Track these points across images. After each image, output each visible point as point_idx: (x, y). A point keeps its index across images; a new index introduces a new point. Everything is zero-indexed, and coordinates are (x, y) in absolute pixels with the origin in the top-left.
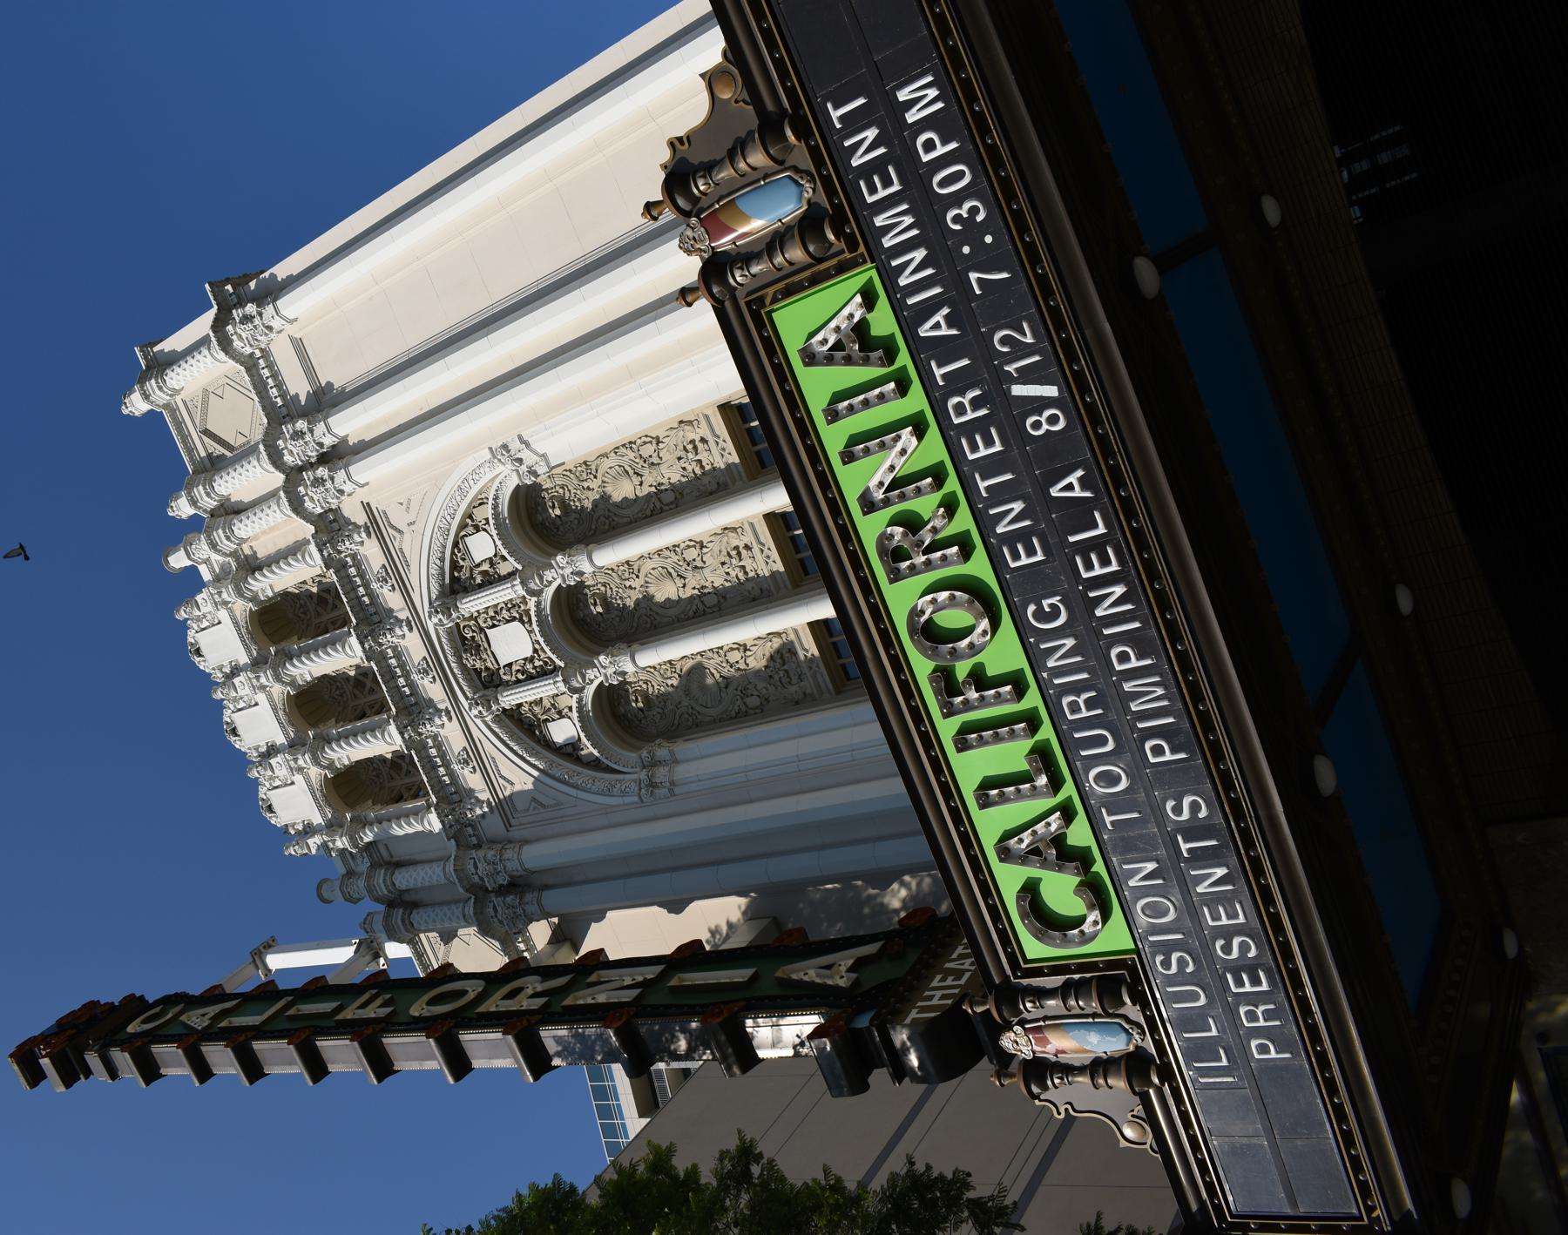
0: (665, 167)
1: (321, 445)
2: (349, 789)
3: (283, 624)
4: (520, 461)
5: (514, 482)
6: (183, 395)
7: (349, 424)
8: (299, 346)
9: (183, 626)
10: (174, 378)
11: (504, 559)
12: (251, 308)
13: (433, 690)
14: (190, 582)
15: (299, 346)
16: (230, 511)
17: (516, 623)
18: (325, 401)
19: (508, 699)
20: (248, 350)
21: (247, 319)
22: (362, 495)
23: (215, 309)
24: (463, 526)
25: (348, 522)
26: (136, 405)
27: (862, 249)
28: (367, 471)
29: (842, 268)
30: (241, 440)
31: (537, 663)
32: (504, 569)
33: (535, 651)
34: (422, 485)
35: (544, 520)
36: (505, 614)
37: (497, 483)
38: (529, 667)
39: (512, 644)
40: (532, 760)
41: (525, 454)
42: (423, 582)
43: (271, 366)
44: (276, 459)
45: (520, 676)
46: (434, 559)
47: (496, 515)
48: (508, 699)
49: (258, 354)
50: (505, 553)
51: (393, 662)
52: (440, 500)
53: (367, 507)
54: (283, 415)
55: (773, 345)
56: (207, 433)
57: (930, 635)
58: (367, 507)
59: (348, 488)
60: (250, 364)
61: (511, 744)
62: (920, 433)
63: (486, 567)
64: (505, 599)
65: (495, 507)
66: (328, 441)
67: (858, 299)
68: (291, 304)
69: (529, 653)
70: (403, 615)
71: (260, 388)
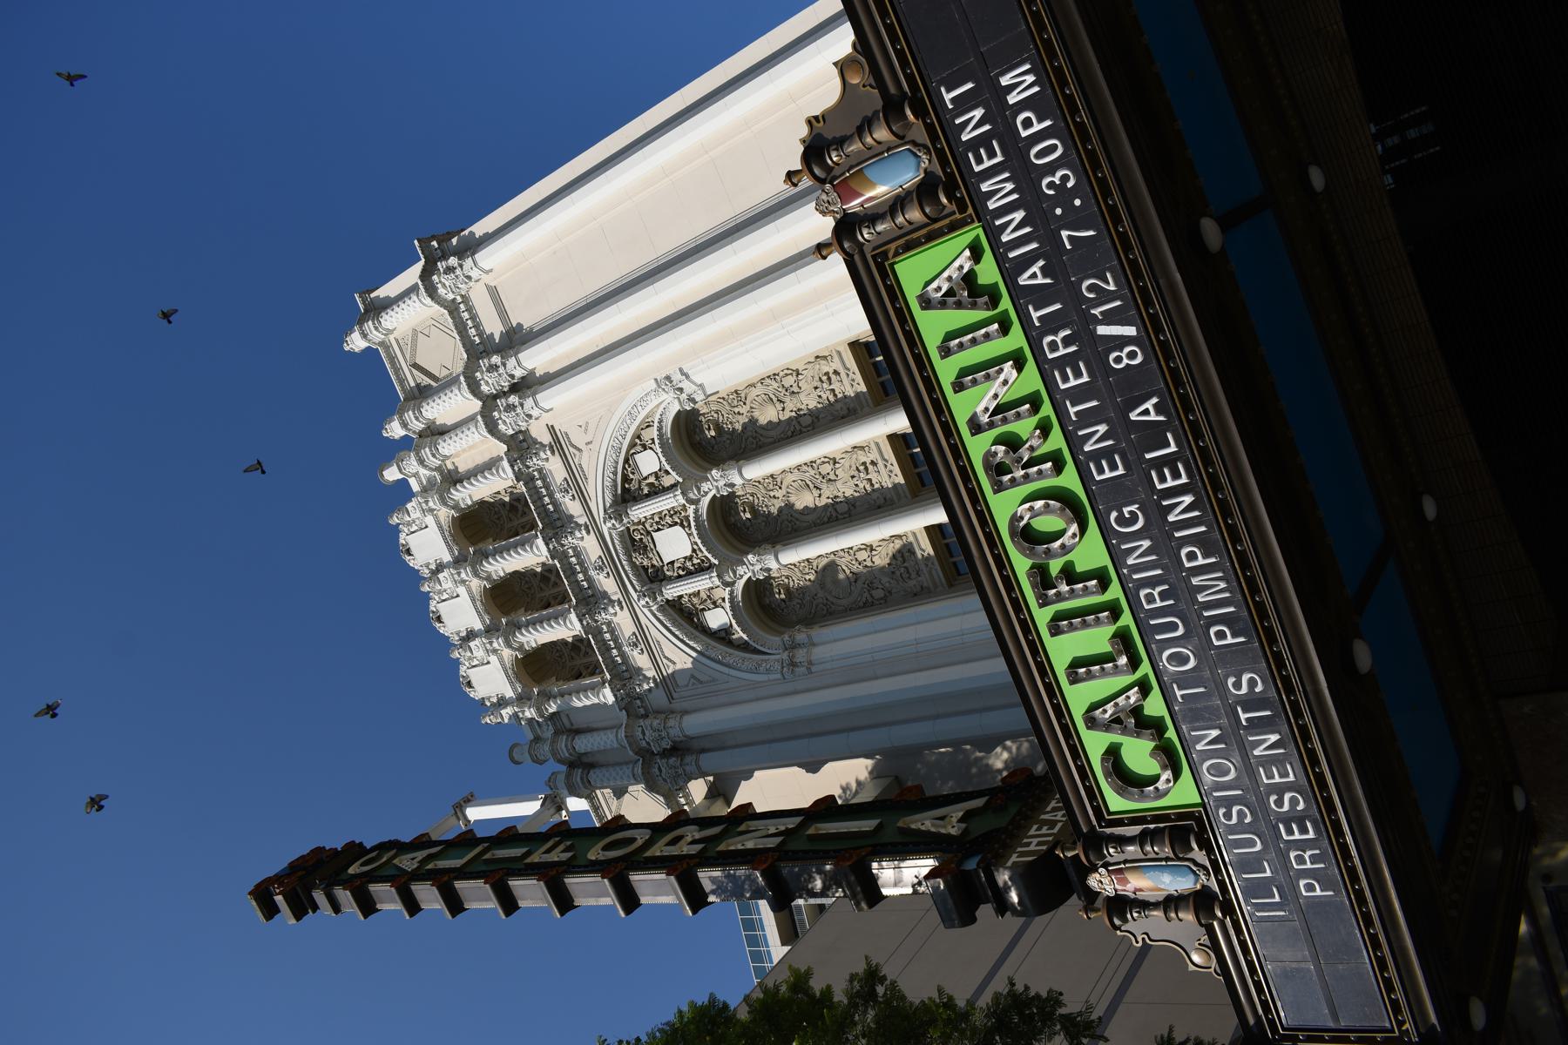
0: (803, 141)
1: (512, 376)
2: (538, 668)
4: (681, 390)
5: (676, 408)
6: (396, 334)
7: (536, 359)
8: (493, 293)
11: (667, 473)
12: (453, 261)
13: (608, 584)
14: (401, 493)
15: (493, 293)
16: (436, 432)
18: (516, 339)
19: (671, 592)
20: (451, 296)
21: (450, 270)
22: (547, 419)
23: (422, 262)
24: (632, 445)
25: (535, 442)
26: (356, 343)
27: (970, 210)
28: (551, 398)
29: (954, 227)
30: (445, 372)
32: (667, 481)
33: (694, 551)
35: (700, 440)
38: (689, 564)
39: (674, 545)
41: (685, 385)
42: (599, 493)
43: (470, 309)
44: (474, 388)
46: (607, 473)
48: (671, 592)
50: (668, 468)
53: (551, 429)
54: (479, 350)
56: (416, 366)
57: (1029, 537)
58: (551, 429)
60: (452, 308)
62: (1019, 366)
63: (652, 480)
66: (519, 373)
67: (967, 253)
69: (689, 553)
70: (582, 520)
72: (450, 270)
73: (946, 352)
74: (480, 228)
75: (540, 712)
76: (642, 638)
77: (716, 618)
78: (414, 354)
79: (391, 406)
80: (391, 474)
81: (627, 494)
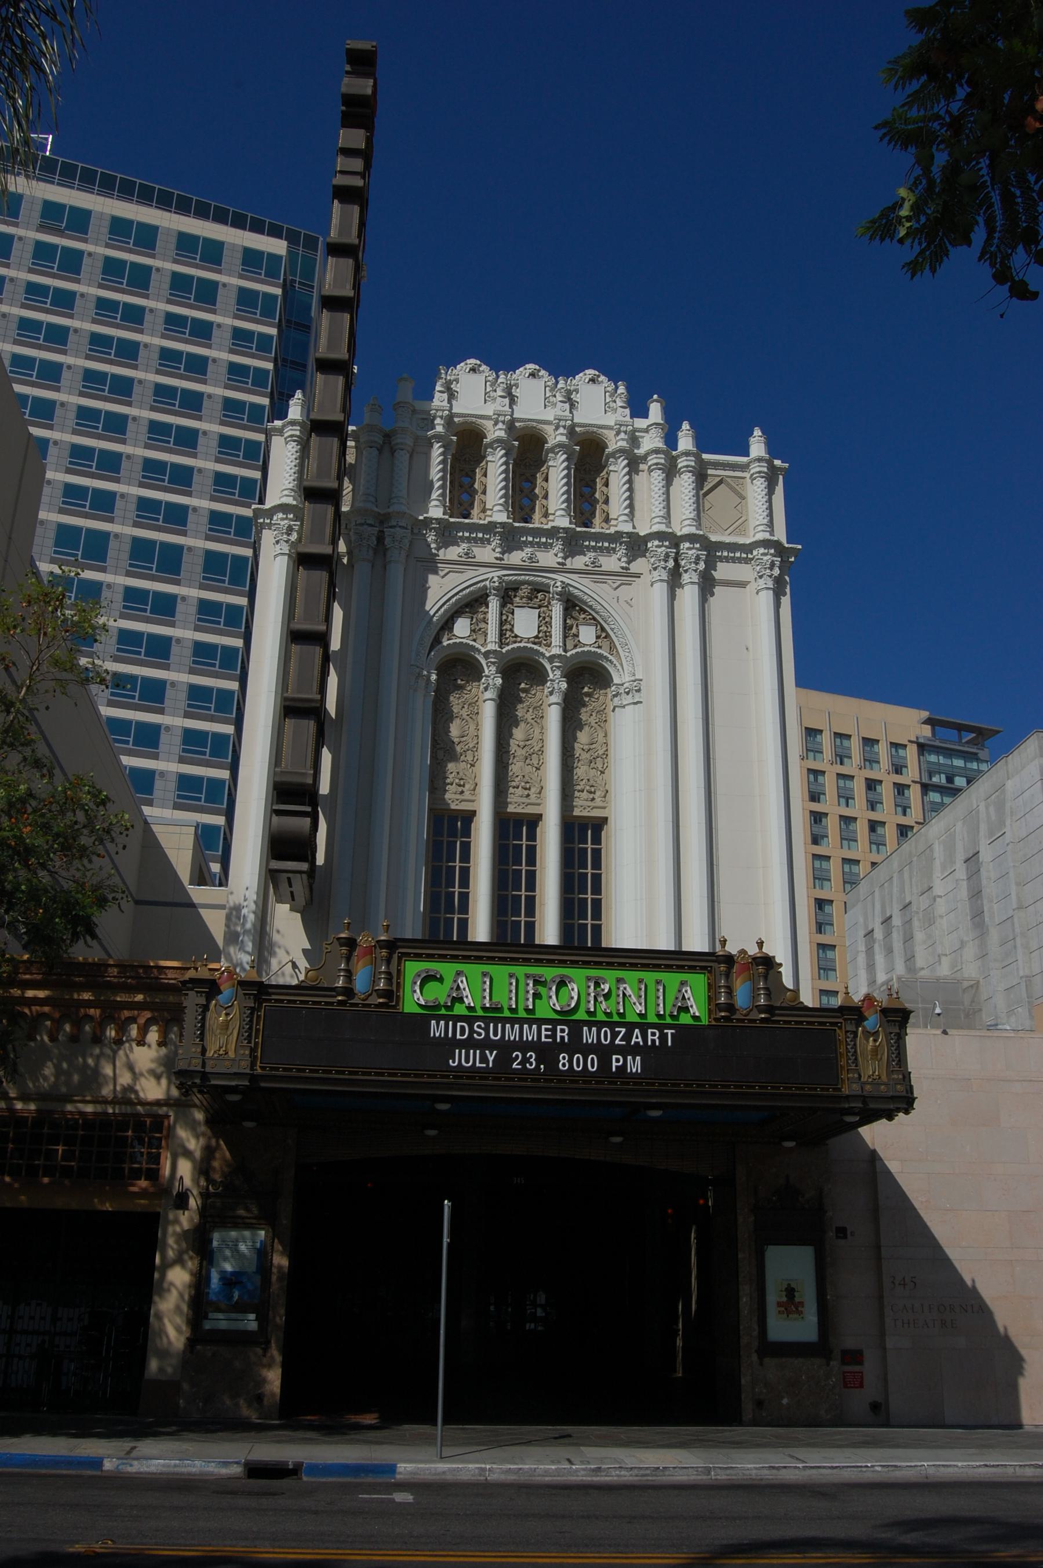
0: (774, 957)
1: (686, 571)
2: (467, 445)
3: (589, 456)
4: (628, 693)
5: (616, 680)
6: (748, 480)
7: (689, 595)
8: (742, 585)
9: (614, 378)
10: (760, 484)
11: (575, 646)
12: (776, 572)
13: (516, 557)
14: (639, 410)
15: (742, 585)
16: (670, 472)
17: (536, 633)
18: (707, 585)
19: (494, 603)
20: (755, 553)
21: (772, 566)
22: (646, 578)
23: (787, 545)
24: (603, 629)
25: (634, 560)
26: (757, 447)
27: (714, 1023)
28: (660, 591)
30: (707, 506)
31: (508, 633)
32: (570, 643)
33: (516, 636)
34: (641, 619)
35: (588, 676)
36: (543, 628)
37: (619, 667)
38: (508, 627)
39: (525, 623)
40: (454, 600)
41: (629, 699)
42: (583, 587)
43: (740, 560)
44: (691, 538)
45: (504, 617)
47: (601, 656)
48: (494, 603)
49: (750, 556)
50: (579, 650)
51: (544, 540)
52: (627, 632)
53: (638, 576)
54: (712, 552)
55: (692, 969)
56: (720, 482)
57: (562, 983)
58: (638, 576)
59: (655, 574)
60: (748, 548)
61: (468, 591)
62: (640, 1015)
63: (574, 630)
64: (553, 633)
65: (606, 658)
66: (686, 578)
67: (697, 1014)
68: (766, 598)
69: (516, 631)
70: (570, 563)
71: (733, 547)
72: (771, 568)
73: (658, 982)
74: (786, 601)
75: (438, 437)
76: (468, 562)
77: (462, 628)
78: (728, 485)
79: (703, 444)
80: (655, 411)
81: (572, 605)
